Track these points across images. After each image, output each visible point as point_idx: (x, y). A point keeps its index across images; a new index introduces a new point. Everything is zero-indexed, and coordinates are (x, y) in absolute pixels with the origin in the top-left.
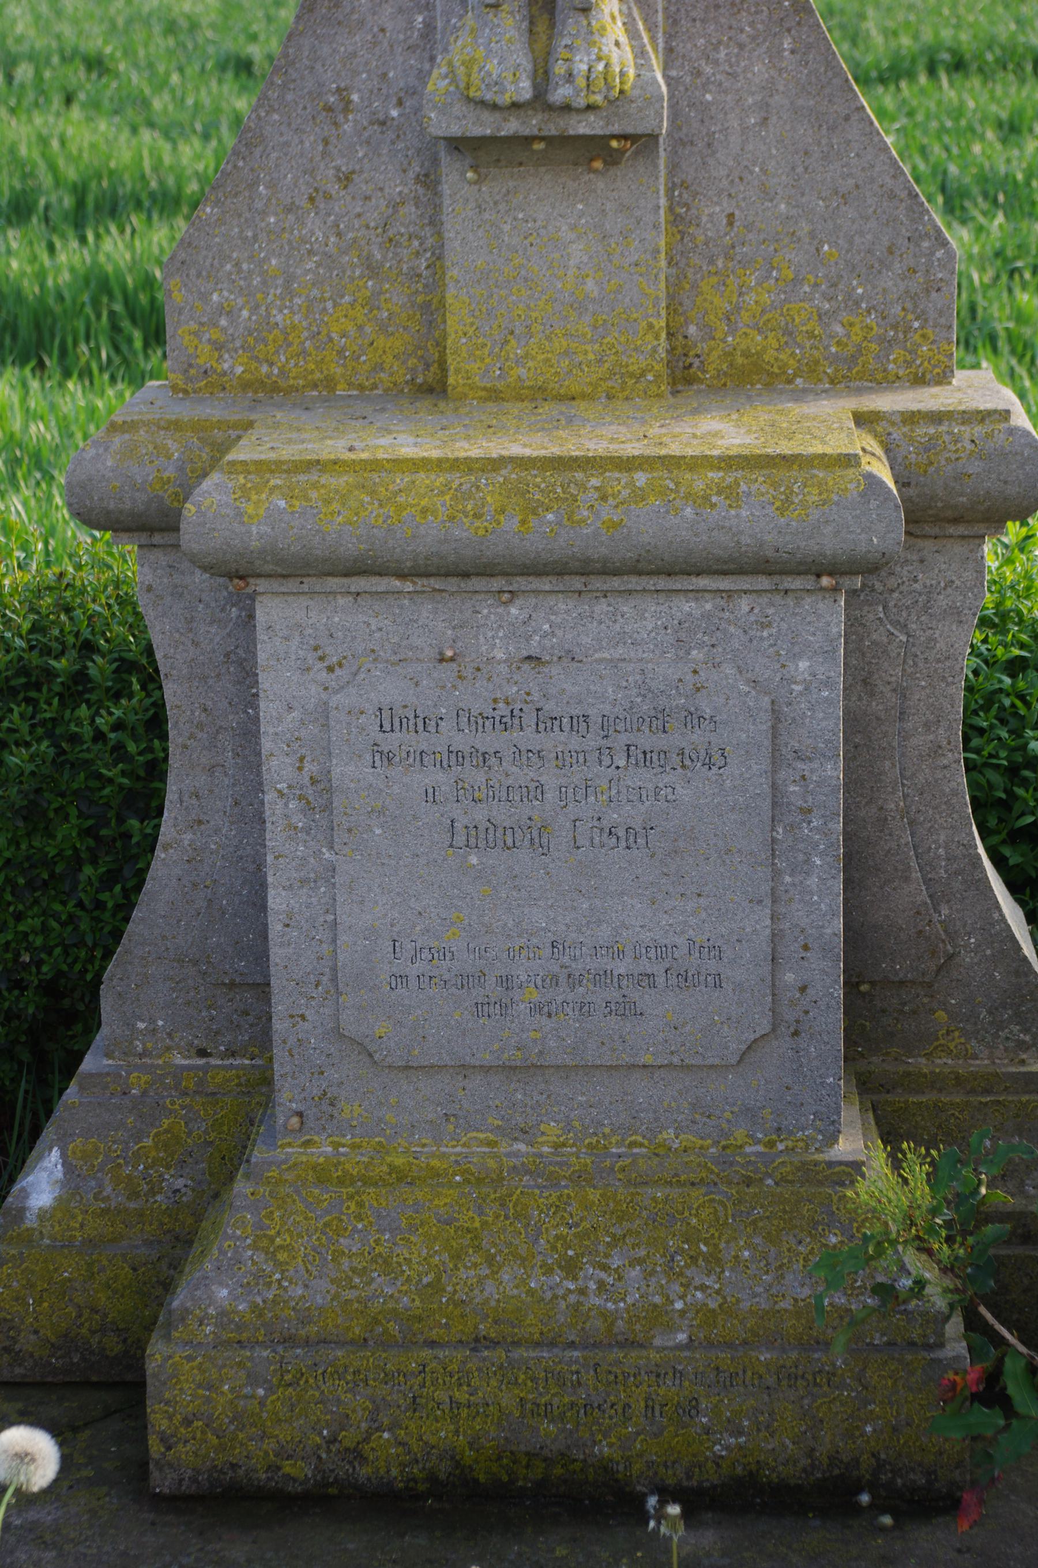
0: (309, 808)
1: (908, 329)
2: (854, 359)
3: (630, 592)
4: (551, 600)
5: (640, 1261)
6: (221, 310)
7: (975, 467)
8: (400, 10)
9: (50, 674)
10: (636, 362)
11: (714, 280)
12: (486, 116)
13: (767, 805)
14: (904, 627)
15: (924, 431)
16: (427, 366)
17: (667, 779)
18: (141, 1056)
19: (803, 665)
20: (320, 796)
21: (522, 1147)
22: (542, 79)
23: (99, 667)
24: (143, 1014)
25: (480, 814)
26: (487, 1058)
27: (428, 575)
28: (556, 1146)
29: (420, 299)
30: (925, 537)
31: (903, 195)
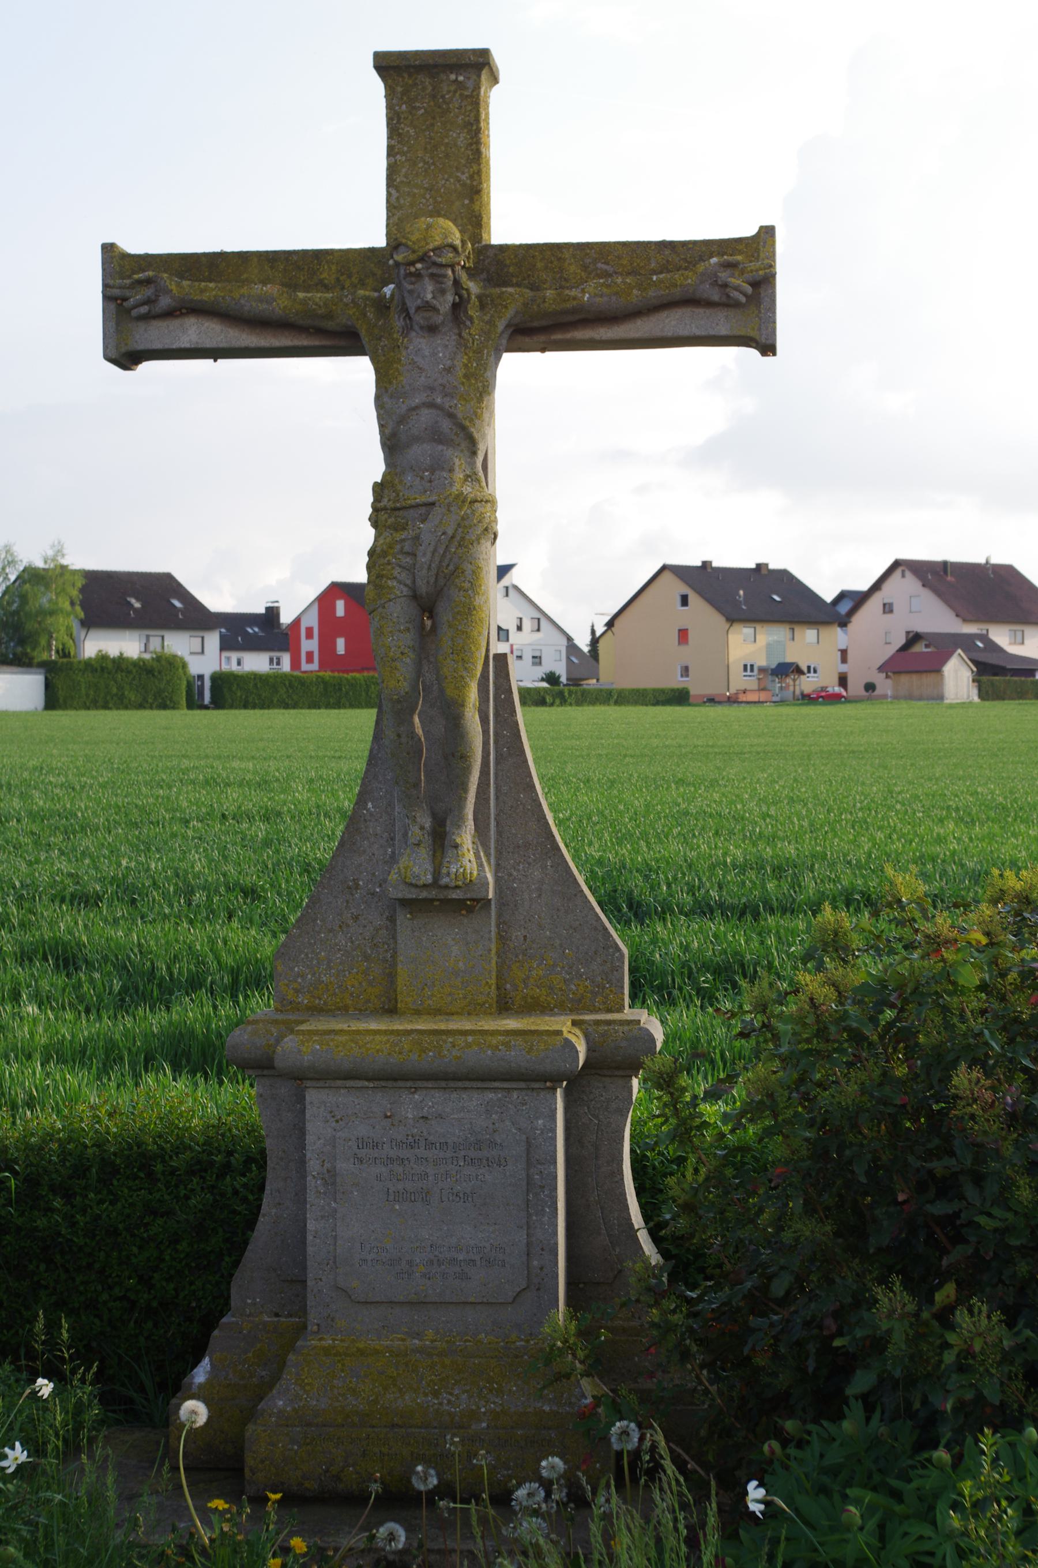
0: (326, 1184)
1: (604, 987)
2: (580, 1001)
3: (466, 1088)
4: (433, 1092)
5: (467, 1391)
6: (299, 975)
7: (624, 1044)
8: (381, 846)
9: (212, 1163)
10: (481, 999)
11: (518, 964)
12: (413, 890)
13: (524, 1183)
14: (597, 1117)
15: (603, 1028)
16: (390, 1001)
17: (481, 1171)
18: (248, 1316)
19: (540, 1122)
20: (331, 1178)
21: (417, 1341)
22: (437, 874)
23: (237, 1160)
24: (250, 1294)
25: (400, 1186)
26: (401, 1298)
27: (380, 1080)
28: (432, 1341)
29: (387, 971)
30: (605, 1076)
31: (601, 928)
